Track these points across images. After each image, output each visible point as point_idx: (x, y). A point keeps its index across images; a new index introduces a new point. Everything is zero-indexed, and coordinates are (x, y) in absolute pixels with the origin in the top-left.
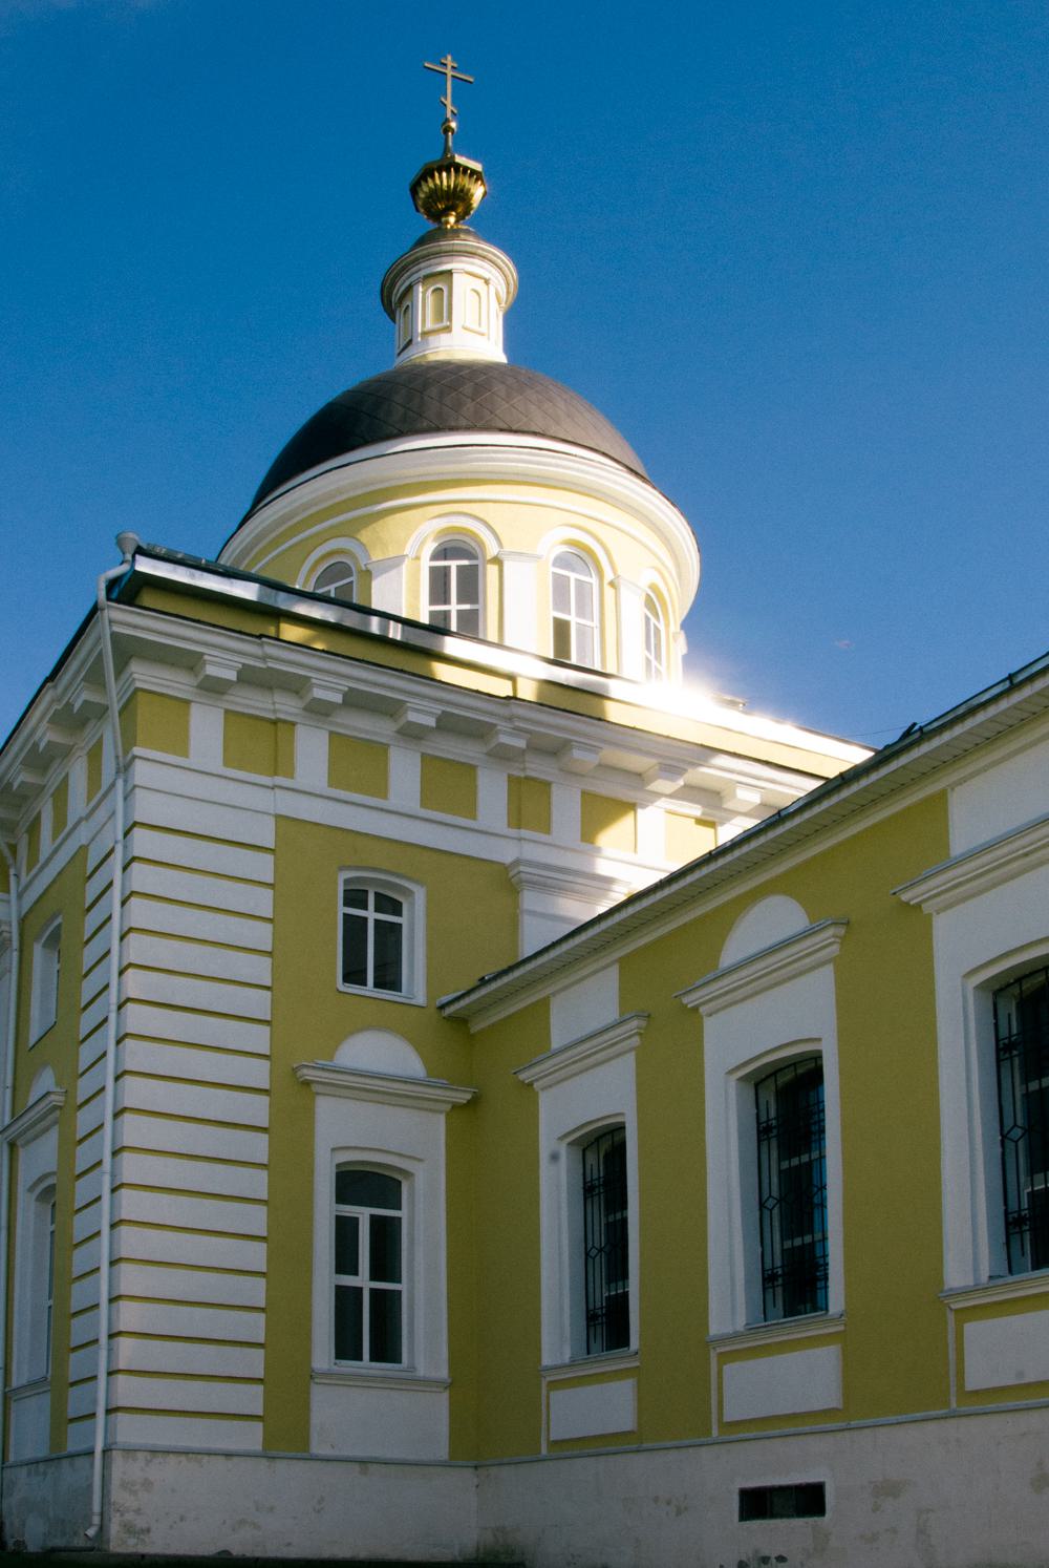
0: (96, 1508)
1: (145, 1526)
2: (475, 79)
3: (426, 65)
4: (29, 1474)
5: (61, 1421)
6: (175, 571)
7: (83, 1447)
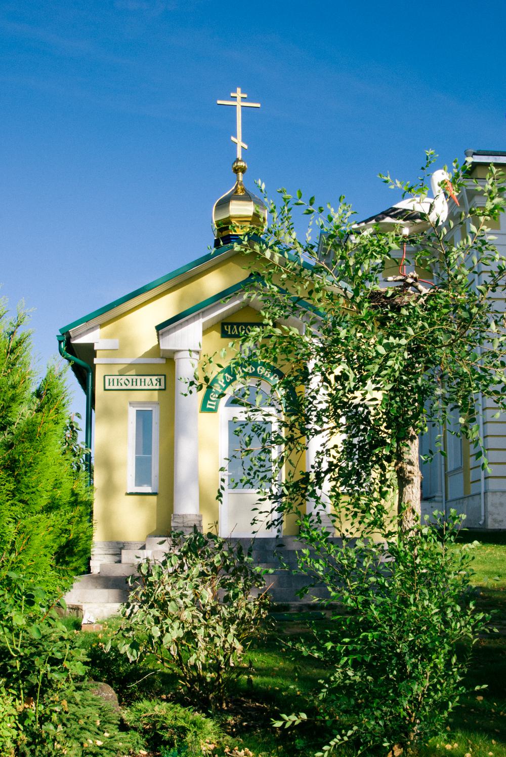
0: (483, 514)
1: (501, 519)
2: (261, 105)
3: (219, 102)
4: (457, 503)
5: (467, 483)
6: (488, 159)
7: (476, 492)
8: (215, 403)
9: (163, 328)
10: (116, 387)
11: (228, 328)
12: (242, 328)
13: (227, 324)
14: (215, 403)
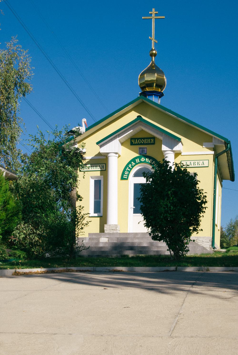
8: (127, 176)
9: (101, 143)
10: (196, 166)
11: (133, 141)
12: (139, 140)
13: (133, 139)
14: (127, 176)
